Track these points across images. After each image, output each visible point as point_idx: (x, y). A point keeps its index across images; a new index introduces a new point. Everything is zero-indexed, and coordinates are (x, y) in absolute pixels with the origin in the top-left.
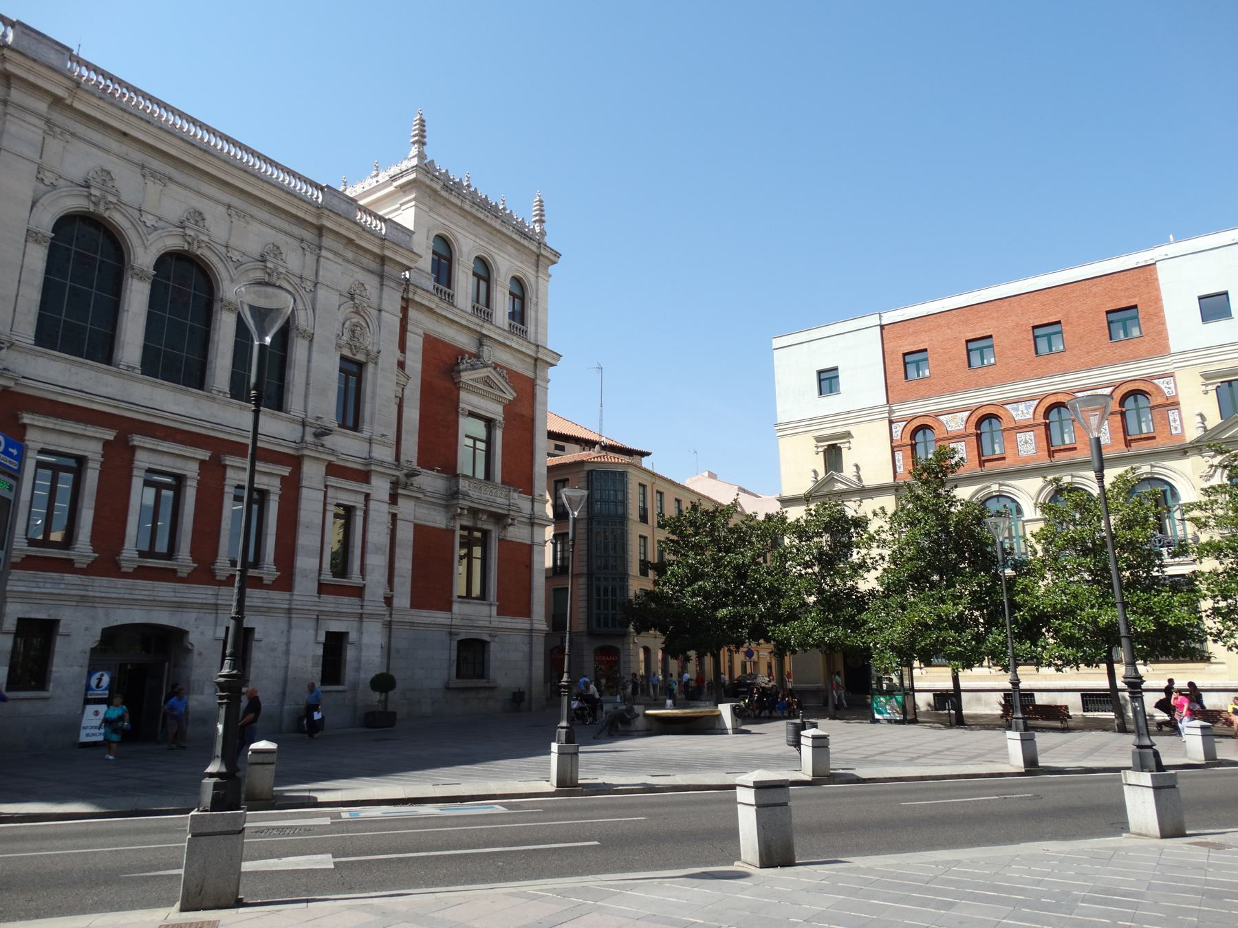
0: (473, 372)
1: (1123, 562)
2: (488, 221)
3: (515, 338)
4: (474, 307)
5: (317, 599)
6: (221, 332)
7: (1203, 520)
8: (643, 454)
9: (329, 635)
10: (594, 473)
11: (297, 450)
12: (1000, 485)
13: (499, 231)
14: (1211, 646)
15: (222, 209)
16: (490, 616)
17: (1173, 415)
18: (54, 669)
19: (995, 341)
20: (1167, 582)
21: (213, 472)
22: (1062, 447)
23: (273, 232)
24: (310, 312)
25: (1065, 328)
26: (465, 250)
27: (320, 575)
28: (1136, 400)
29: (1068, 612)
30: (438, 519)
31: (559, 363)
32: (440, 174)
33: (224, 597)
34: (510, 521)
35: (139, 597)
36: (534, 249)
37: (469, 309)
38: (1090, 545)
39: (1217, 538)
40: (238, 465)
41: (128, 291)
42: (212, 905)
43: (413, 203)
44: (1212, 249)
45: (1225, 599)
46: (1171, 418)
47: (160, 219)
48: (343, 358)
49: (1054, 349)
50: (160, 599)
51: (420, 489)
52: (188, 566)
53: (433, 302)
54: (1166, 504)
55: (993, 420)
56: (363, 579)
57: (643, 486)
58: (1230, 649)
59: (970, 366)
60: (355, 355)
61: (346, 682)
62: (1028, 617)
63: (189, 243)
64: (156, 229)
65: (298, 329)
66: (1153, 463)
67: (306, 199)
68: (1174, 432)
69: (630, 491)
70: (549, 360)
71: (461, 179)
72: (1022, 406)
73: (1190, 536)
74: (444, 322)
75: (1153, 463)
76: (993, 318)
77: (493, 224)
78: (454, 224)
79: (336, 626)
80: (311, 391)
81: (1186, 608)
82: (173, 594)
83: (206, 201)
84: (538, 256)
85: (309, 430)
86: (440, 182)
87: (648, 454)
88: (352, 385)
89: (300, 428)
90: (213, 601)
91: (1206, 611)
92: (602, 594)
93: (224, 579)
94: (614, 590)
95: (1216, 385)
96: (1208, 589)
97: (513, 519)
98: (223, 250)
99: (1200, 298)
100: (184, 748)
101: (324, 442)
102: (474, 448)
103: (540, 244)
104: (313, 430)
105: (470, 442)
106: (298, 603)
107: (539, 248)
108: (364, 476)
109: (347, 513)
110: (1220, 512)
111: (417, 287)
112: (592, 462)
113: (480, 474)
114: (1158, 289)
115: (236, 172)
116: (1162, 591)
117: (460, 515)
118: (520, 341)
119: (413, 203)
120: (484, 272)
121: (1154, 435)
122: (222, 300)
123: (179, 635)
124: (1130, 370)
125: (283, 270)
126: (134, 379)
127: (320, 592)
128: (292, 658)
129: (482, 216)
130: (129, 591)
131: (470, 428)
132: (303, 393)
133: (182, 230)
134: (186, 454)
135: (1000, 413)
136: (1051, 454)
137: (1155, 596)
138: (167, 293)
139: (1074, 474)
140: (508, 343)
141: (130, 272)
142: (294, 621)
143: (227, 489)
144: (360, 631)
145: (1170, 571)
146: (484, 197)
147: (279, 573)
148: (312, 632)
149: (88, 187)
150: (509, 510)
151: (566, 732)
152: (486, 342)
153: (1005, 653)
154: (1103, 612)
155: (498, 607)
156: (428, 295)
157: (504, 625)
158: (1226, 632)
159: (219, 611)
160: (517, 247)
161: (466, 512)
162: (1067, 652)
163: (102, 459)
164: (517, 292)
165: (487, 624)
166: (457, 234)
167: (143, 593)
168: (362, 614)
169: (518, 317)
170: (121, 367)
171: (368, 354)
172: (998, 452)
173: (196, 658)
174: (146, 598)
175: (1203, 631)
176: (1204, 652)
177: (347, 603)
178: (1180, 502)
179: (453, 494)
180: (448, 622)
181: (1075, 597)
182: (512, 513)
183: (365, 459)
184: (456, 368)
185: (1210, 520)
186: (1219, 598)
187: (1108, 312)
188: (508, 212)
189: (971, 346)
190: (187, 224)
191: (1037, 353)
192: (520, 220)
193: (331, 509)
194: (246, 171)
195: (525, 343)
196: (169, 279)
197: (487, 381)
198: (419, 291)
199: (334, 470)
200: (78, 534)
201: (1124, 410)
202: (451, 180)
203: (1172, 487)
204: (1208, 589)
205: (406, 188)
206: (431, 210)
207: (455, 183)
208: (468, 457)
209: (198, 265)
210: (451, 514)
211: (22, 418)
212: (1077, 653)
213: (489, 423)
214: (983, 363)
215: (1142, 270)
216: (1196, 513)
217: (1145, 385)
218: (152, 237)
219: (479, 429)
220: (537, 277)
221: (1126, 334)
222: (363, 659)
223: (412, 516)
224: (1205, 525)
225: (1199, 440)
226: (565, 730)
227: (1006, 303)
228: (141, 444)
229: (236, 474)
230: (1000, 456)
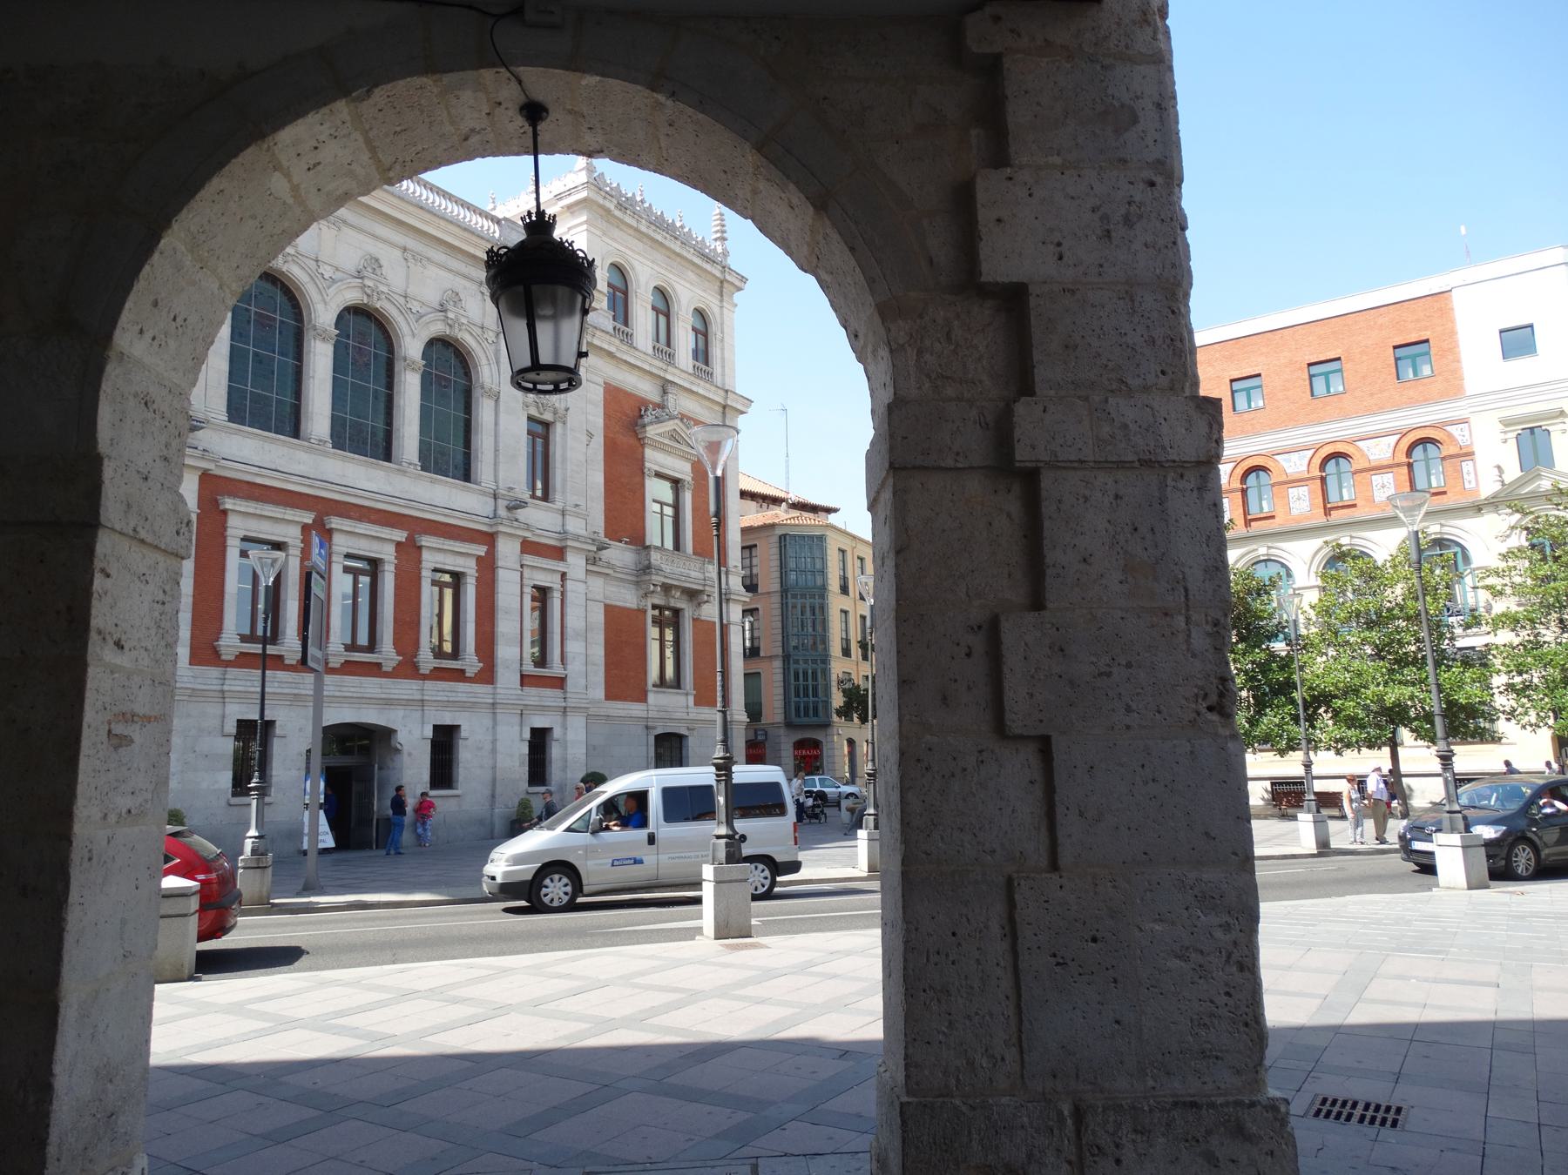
0: (659, 425)
1: (1412, 636)
2: (667, 243)
3: (702, 383)
4: (654, 348)
5: (520, 692)
6: (406, 396)
7: (1499, 588)
8: (829, 510)
9: (534, 731)
10: (788, 537)
11: (491, 526)
12: (1269, 548)
13: (678, 255)
14: (1502, 726)
15: (397, 253)
16: (687, 708)
17: (1467, 466)
18: (274, 773)
19: (1264, 380)
20: (1458, 656)
21: (409, 552)
22: (1340, 504)
23: (450, 276)
24: (494, 367)
25: (1347, 366)
26: (643, 280)
27: (521, 665)
28: (1425, 450)
29: (1352, 691)
30: (628, 598)
31: (750, 410)
32: (611, 189)
33: (430, 693)
34: (706, 598)
35: (350, 694)
36: (718, 274)
37: (650, 351)
38: (1374, 617)
39: (1514, 608)
40: (434, 545)
41: (312, 355)
42: (736, 935)
43: (585, 227)
44: (1517, 274)
45: (1520, 673)
46: (1465, 471)
47: (337, 269)
48: (530, 419)
49: (1332, 390)
50: (368, 696)
51: (609, 565)
52: (392, 659)
53: (612, 344)
54: (1457, 570)
55: (1261, 473)
56: (565, 670)
57: (843, 551)
58: (1524, 727)
59: (1234, 410)
60: (542, 414)
61: (553, 783)
62: (1307, 697)
63: (368, 295)
64: (334, 281)
65: (483, 388)
66: (1443, 522)
67: (406, 198)
68: (1467, 486)
69: (829, 558)
70: (740, 407)
71: (634, 194)
72: (1294, 456)
73: (1482, 604)
74: (625, 367)
75: (1443, 522)
76: (1262, 354)
77: (672, 246)
78: (630, 249)
79: (540, 722)
80: (501, 459)
81: (1478, 685)
82: (380, 690)
83: (381, 245)
84: (722, 282)
85: (502, 503)
86: (613, 200)
87: (835, 510)
88: (539, 448)
89: (491, 501)
90: (419, 697)
91: (1498, 687)
92: (810, 679)
93: (232, 658)
94: (814, 673)
95: (1516, 433)
96: (1503, 664)
97: (708, 596)
98: (402, 300)
99: (1501, 332)
100: (400, 853)
101: (518, 517)
102: (662, 514)
103: (724, 267)
104: (506, 503)
105: (657, 507)
106: (502, 696)
107: (723, 272)
108: (559, 553)
109: (542, 594)
110: (1518, 580)
111: (596, 328)
112: (785, 525)
113: (669, 544)
114: (1453, 321)
115: (411, 209)
116: (1452, 667)
117: (653, 592)
118: (708, 386)
119: (585, 227)
120: (664, 304)
121: (1445, 489)
122: (405, 359)
123: (386, 734)
125: (464, 320)
126: (325, 454)
127: (522, 684)
128: (499, 757)
129: (659, 238)
130: (338, 688)
131: (657, 491)
132: (492, 462)
133: (360, 281)
134: (383, 536)
136: (1327, 511)
137: (1445, 672)
138: (348, 354)
139: (1354, 534)
140: (695, 388)
141: (312, 333)
142: (499, 717)
143: (230, 542)
144: (565, 727)
145: (1460, 643)
146: (659, 213)
147: (481, 665)
148: (517, 728)
149: (445, 311)
150: (705, 585)
151: (727, 844)
152: (670, 389)
153: (1281, 736)
154: (1388, 689)
155: (695, 696)
156: (608, 337)
157: (703, 717)
158: (1520, 710)
159: (227, 700)
160: (698, 271)
161: (659, 589)
162: (1349, 733)
163: (302, 545)
164: (618, 283)
165: (684, 716)
166: (633, 262)
167: (352, 689)
168: (565, 708)
169: (701, 357)
170: (312, 441)
171: (555, 413)
172: (1266, 509)
173: (405, 757)
174: (355, 695)
175: (1495, 709)
176: (1495, 732)
177: (550, 696)
178: (1472, 566)
179: (646, 569)
180: (644, 714)
181: (1360, 675)
182: (707, 588)
183: (560, 533)
184: (640, 421)
185: (1506, 588)
186: (1514, 673)
187: (1395, 347)
188: (686, 230)
189: (1236, 386)
190: (366, 274)
191: (1312, 395)
192: (615, 185)
193: (528, 590)
194: (421, 208)
195: (713, 388)
196: (348, 338)
197: (674, 436)
198: (598, 333)
199: (529, 547)
200: (285, 627)
201: (1411, 461)
202: (607, 185)
203: (1463, 548)
204: (1503, 664)
205: (575, 209)
206: (604, 234)
207: (627, 199)
208: (657, 529)
209: (376, 319)
210: (642, 592)
211: (224, 503)
212: (1361, 734)
213: (676, 483)
214: (1250, 407)
215: (1435, 298)
216: (1491, 581)
217: (1436, 433)
218: (332, 291)
219: (663, 490)
220: (721, 307)
221: (1415, 374)
222: (570, 757)
223: (602, 595)
224: (1501, 593)
226: (724, 841)
227: (1278, 335)
228: (339, 527)
229: (437, 555)
230: (1269, 515)
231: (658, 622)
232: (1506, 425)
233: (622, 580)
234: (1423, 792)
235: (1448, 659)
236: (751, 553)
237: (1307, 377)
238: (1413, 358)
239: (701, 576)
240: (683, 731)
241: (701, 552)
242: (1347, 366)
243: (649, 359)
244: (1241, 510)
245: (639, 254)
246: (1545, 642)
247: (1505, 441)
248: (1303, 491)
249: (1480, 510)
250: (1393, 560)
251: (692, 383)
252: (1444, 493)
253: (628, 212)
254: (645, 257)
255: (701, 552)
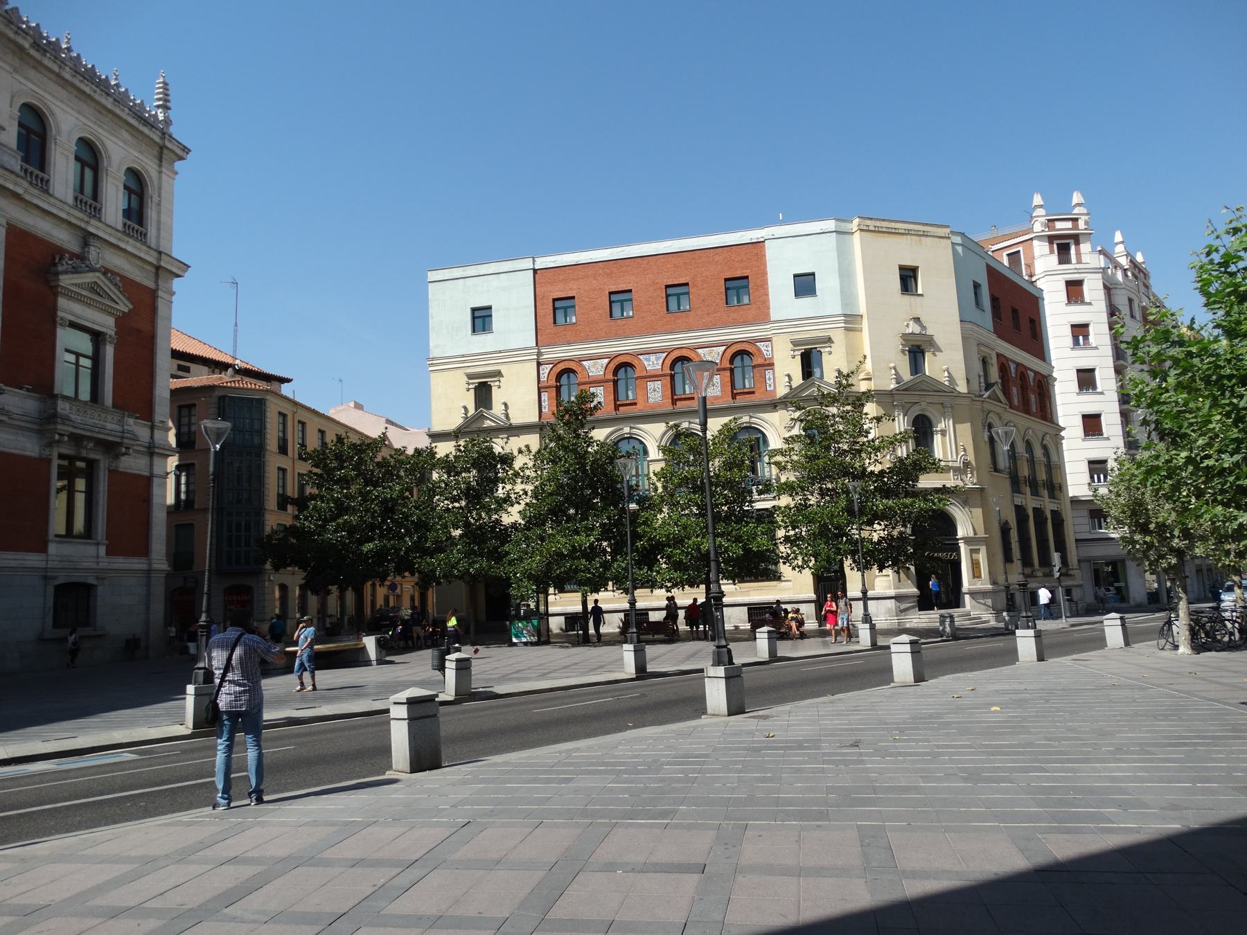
0: (76, 275)
2: (97, 97)
3: (131, 241)
13: (110, 111)
14: (784, 569)
17: (769, 374)
19: (634, 295)
22: (683, 397)
26: (64, 127)
29: (678, 541)
34: (124, 450)
36: (157, 139)
37: (70, 200)
39: (793, 479)
49: (682, 308)
57: (283, 416)
59: (611, 316)
69: (268, 420)
70: (175, 270)
72: (653, 357)
74: (36, 212)
76: (633, 274)
77: (103, 101)
87: (288, 381)
96: (782, 521)
99: (795, 276)
102: (77, 364)
105: (72, 358)
107: (163, 138)
110: (795, 458)
112: (225, 387)
114: (765, 265)
117: (59, 441)
118: (138, 244)
124: (740, 333)
129: (87, 90)
131: (70, 342)
135: (635, 362)
136: (674, 402)
137: (744, 527)
140: (123, 245)
154: (705, 540)
156: (13, 177)
157: (116, 566)
161: (66, 439)
164: (32, 124)
165: (94, 566)
166: (53, 107)
180: (42, 565)
181: (685, 528)
182: (126, 441)
187: (726, 280)
189: (614, 298)
191: (668, 310)
204: (782, 521)
207: (49, 43)
213: (97, 337)
214: (622, 315)
215: (754, 246)
216: (779, 458)
219: (83, 343)
221: (738, 302)
224: (785, 468)
225: (785, 397)
226: (202, 671)
231: (68, 474)
232: (795, 345)
233: (20, 428)
234: (729, 618)
235: (747, 517)
236: (190, 412)
237: (664, 296)
238: (738, 289)
239: (118, 428)
240: (91, 581)
241: (121, 405)
242: (692, 290)
243: (67, 208)
244: (612, 397)
245: (61, 101)
246: (810, 505)
247: (794, 357)
248: (658, 384)
249: (776, 407)
250: (714, 439)
251: (119, 239)
252: (753, 393)
253: (48, 55)
254: (68, 105)
255: (121, 405)
